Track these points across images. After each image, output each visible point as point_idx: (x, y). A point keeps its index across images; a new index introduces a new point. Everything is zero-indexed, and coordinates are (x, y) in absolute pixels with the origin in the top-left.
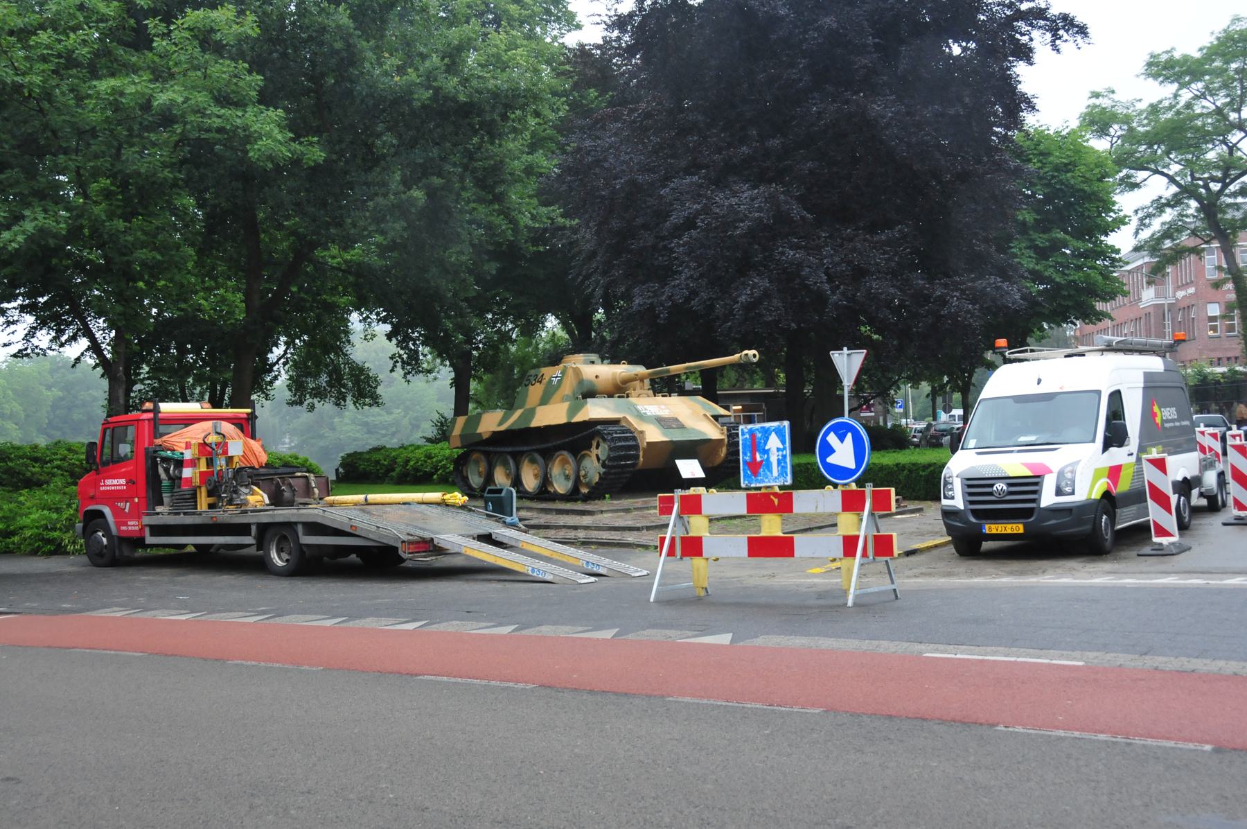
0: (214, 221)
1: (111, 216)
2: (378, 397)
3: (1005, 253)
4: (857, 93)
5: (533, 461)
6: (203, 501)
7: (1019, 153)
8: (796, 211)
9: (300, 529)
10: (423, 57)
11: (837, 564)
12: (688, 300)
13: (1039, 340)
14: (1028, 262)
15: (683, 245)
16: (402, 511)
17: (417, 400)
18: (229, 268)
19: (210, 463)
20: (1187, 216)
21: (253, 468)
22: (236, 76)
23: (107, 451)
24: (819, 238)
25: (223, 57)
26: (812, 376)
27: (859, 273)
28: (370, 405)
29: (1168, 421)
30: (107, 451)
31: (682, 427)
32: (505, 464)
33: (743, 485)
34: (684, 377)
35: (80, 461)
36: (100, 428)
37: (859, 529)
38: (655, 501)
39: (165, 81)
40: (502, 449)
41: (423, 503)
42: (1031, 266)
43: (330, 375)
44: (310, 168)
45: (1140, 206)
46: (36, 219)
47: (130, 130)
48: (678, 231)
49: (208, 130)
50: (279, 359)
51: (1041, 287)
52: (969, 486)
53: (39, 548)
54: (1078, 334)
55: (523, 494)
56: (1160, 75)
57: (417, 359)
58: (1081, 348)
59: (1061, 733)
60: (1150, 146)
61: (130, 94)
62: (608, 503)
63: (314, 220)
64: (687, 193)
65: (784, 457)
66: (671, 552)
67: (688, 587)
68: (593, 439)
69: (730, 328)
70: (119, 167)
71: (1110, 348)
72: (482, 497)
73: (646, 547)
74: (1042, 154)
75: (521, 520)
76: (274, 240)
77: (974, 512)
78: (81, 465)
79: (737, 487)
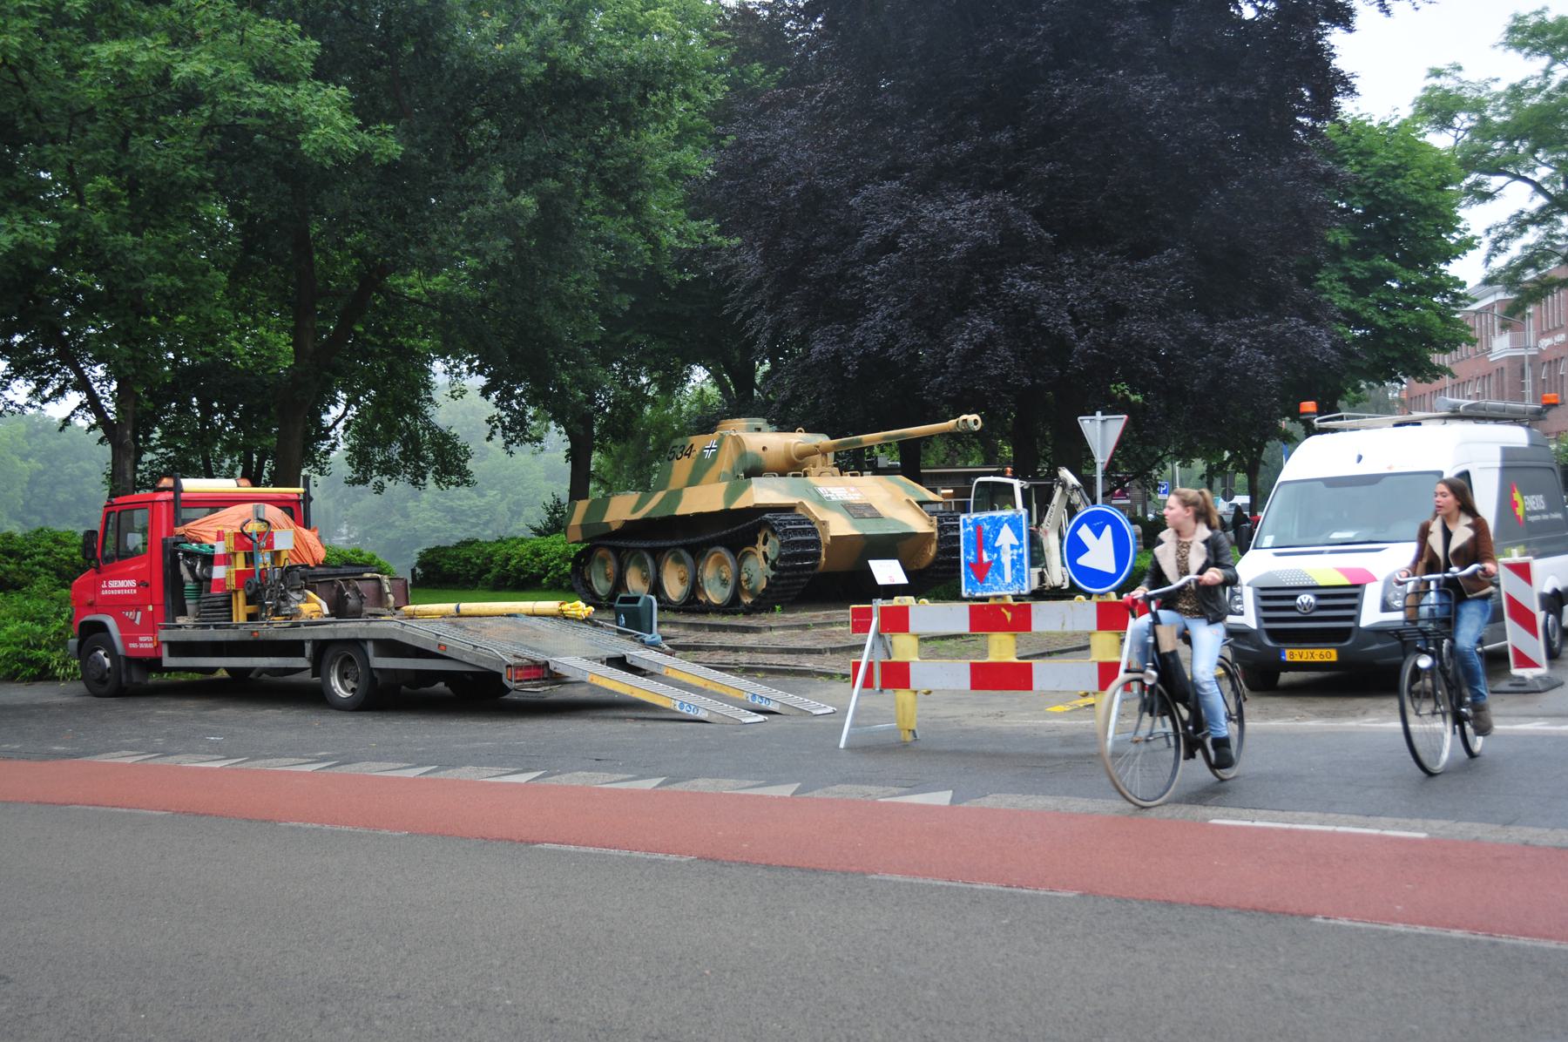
0: (252, 234)
1: (115, 228)
2: (468, 473)
3: (1310, 287)
4: (1113, 71)
5: (678, 560)
6: (240, 611)
7: (1330, 150)
8: (1031, 229)
9: (370, 647)
10: (535, 18)
11: (1090, 700)
12: (884, 347)
13: (1353, 405)
14: (1341, 300)
15: (880, 274)
16: (506, 624)
17: (521, 478)
18: (271, 299)
19: (250, 559)
20: (1558, 237)
21: (307, 566)
22: (283, 41)
23: (110, 543)
24: (1061, 265)
25: (263, 14)
26: (1048, 450)
27: (1116, 312)
28: (458, 485)
29: (1533, 513)
30: (110, 543)
31: (878, 516)
32: (641, 564)
33: (964, 594)
34: (876, 450)
35: (71, 556)
36: (101, 512)
37: (1120, 654)
38: (847, 614)
39: (187, 46)
40: (638, 544)
41: (534, 615)
42: (1345, 304)
43: (405, 445)
44: (382, 166)
45: (1491, 225)
46: (14, 230)
47: (140, 111)
48: (872, 254)
49: (245, 114)
50: (336, 422)
51: (1358, 333)
52: (1264, 598)
53: (17, 672)
54: (1404, 396)
55: (666, 605)
56: (1525, 45)
57: (523, 424)
58: (1417, 415)
59: (1401, 928)
60: (1509, 141)
61: (142, 63)
62: (778, 617)
63: (388, 236)
64: (885, 203)
65: (1020, 556)
66: (868, 683)
67: (889, 730)
69: (942, 384)
70: (126, 162)
71: (1456, 415)
72: (610, 608)
73: (830, 676)
74: (1361, 153)
75: (664, 638)
76: (331, 262)
77: (1272, 634)
78: (72, 563)
79: (956, 596)
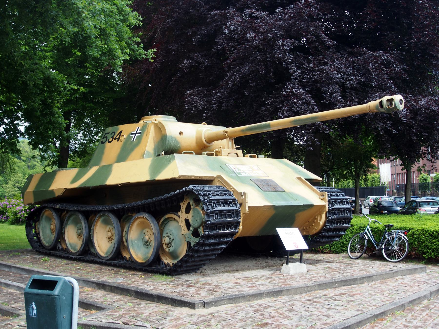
68: (182, 200)
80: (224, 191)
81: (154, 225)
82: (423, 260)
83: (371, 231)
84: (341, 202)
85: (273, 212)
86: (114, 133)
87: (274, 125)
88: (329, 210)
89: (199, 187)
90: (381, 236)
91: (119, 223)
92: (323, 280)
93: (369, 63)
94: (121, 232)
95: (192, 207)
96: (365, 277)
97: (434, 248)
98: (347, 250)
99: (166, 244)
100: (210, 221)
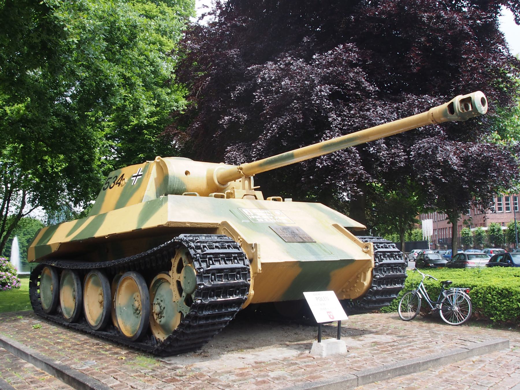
68: (172, 255)
80: (227, 242)
81: (142, 288)
82: (490, 323)
83: (426, 288)
84: (391, 255)
85: (298, 270)
86: (116, 177)
87: (299, 155)
88: (375, 266)
89: (191, 236)
90: (438, 295)
91: (108, 285)
92: (369, 368)
93: (415, 108)
94: (110, 296)
95: (184, 265)
96: (430, 361)
97: (504, 310)
98: (397, 309)
99: (156, 314)
100: (203, 284)
